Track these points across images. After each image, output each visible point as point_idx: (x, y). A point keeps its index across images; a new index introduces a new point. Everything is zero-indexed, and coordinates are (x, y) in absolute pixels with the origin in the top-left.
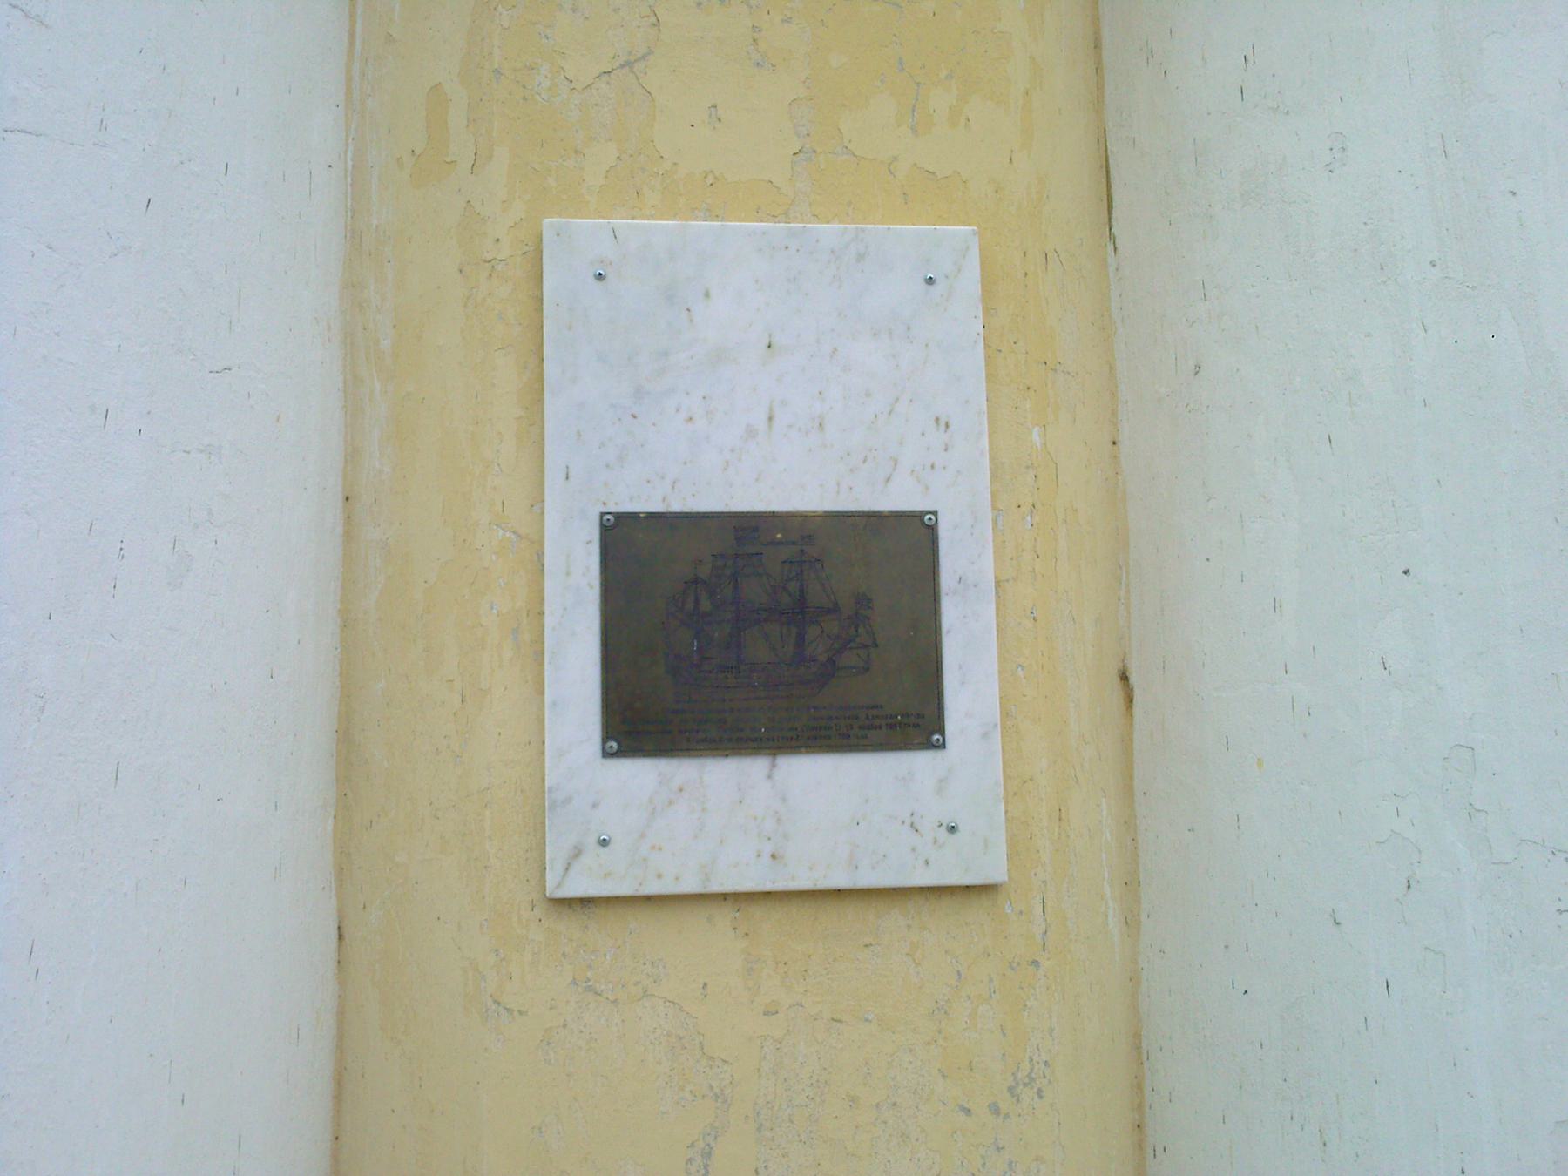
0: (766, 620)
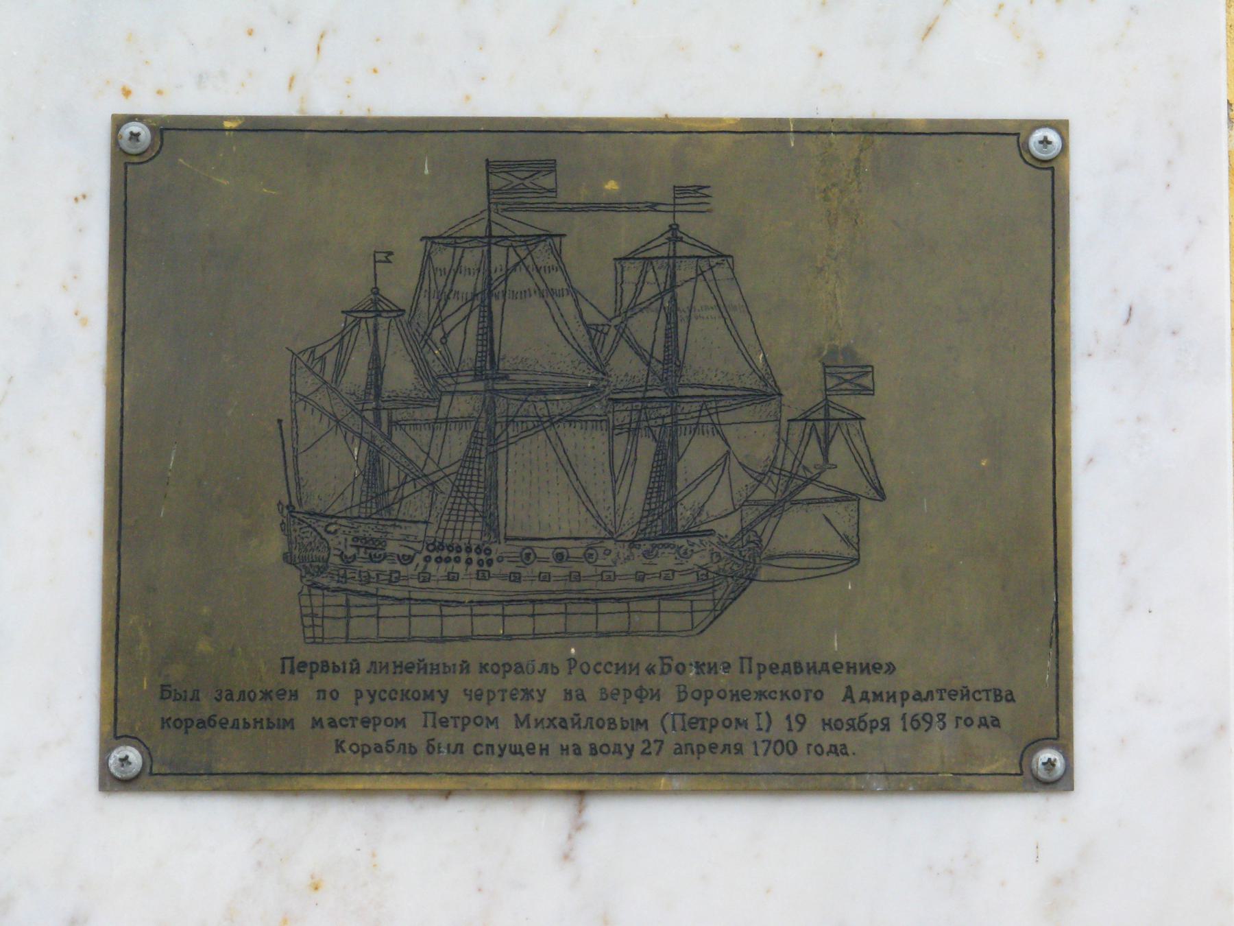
0: (568, 418)
